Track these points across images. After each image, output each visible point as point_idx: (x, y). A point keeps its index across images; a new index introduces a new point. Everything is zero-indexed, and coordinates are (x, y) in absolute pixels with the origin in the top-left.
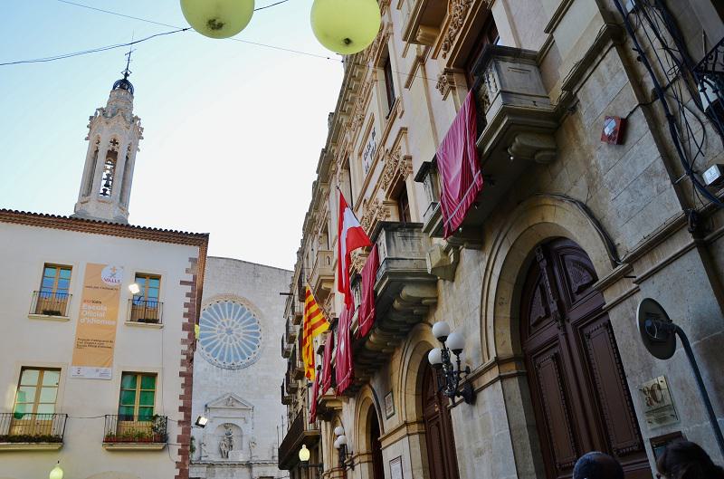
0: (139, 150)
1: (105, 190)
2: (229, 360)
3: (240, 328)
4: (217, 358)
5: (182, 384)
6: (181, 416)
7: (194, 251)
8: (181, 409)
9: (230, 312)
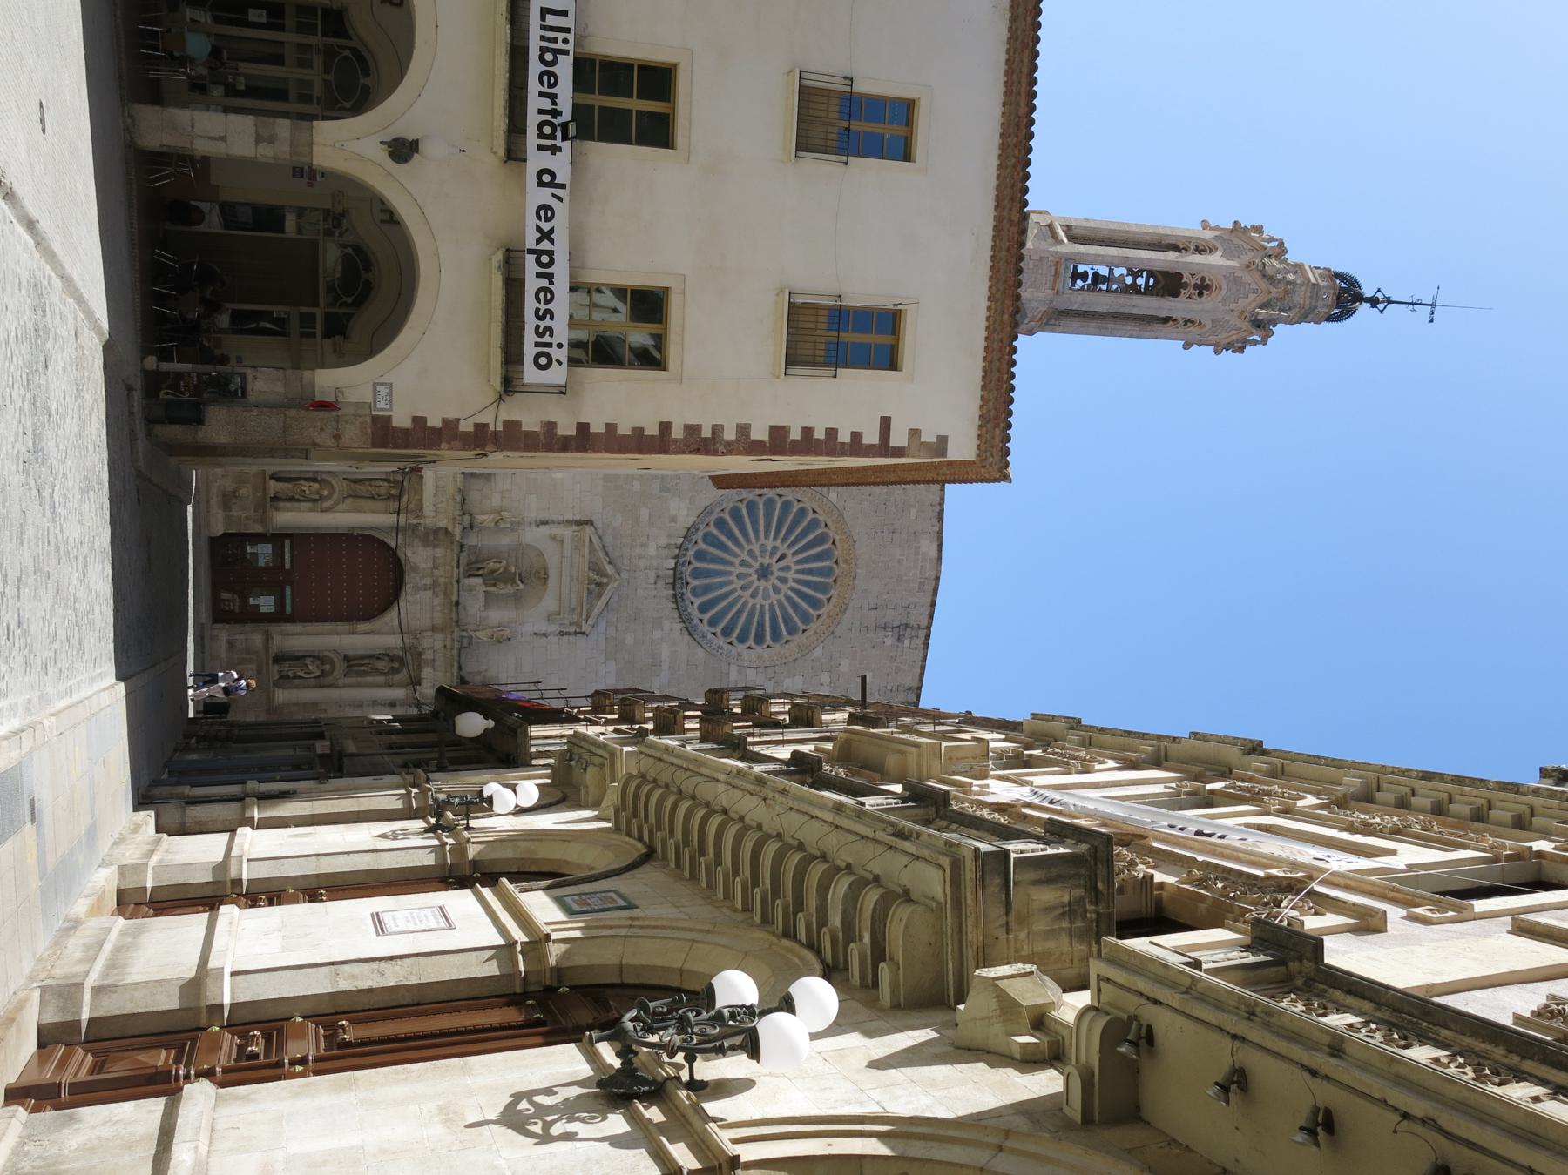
0: (1187, 346)
1: (1084, 276)
2: (697, 574)
3: (774, 597)
4: (701, 546)
5: (642, 430)
6: (566, 428)
7: (963, 448)
8: (583, 428)
9: (811, 572)
